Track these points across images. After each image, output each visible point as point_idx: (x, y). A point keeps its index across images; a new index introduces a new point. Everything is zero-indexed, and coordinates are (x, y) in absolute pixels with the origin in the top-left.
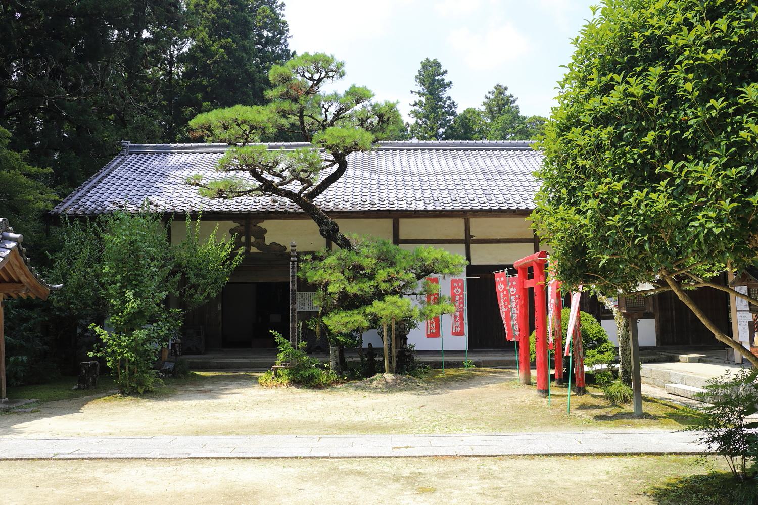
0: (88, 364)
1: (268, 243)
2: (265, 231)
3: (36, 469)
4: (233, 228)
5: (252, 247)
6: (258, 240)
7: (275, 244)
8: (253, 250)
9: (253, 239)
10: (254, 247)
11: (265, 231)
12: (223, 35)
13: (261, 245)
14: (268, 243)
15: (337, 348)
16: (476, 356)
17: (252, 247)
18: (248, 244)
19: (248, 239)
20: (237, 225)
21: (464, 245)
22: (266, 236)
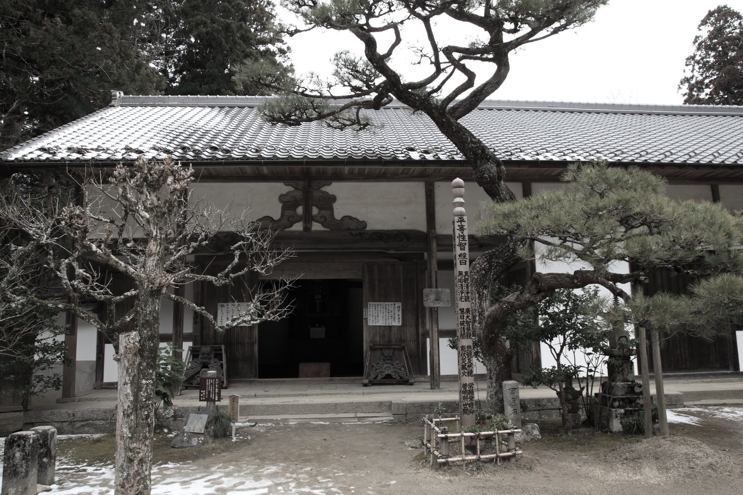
0: (25, 438)
1: (338, 215)
2: (333, 199)
3: (646, 427)
4: (284, 193)
5: (314, 223)
6: (323, 212)
7: (350, 218)
8: (316, 227)
9: (315, 211)
10: (317, 221)
11: (333, 199)
12: (547, 17)
13: (327, 219)
14: (338, 215)
15: (542, 344)
16: (272, 390)
17: (314, 223)
18: (308, 218)
19: (307, 210)
20: (290, 189)
21: (437, 184)
22: (335, 205)
